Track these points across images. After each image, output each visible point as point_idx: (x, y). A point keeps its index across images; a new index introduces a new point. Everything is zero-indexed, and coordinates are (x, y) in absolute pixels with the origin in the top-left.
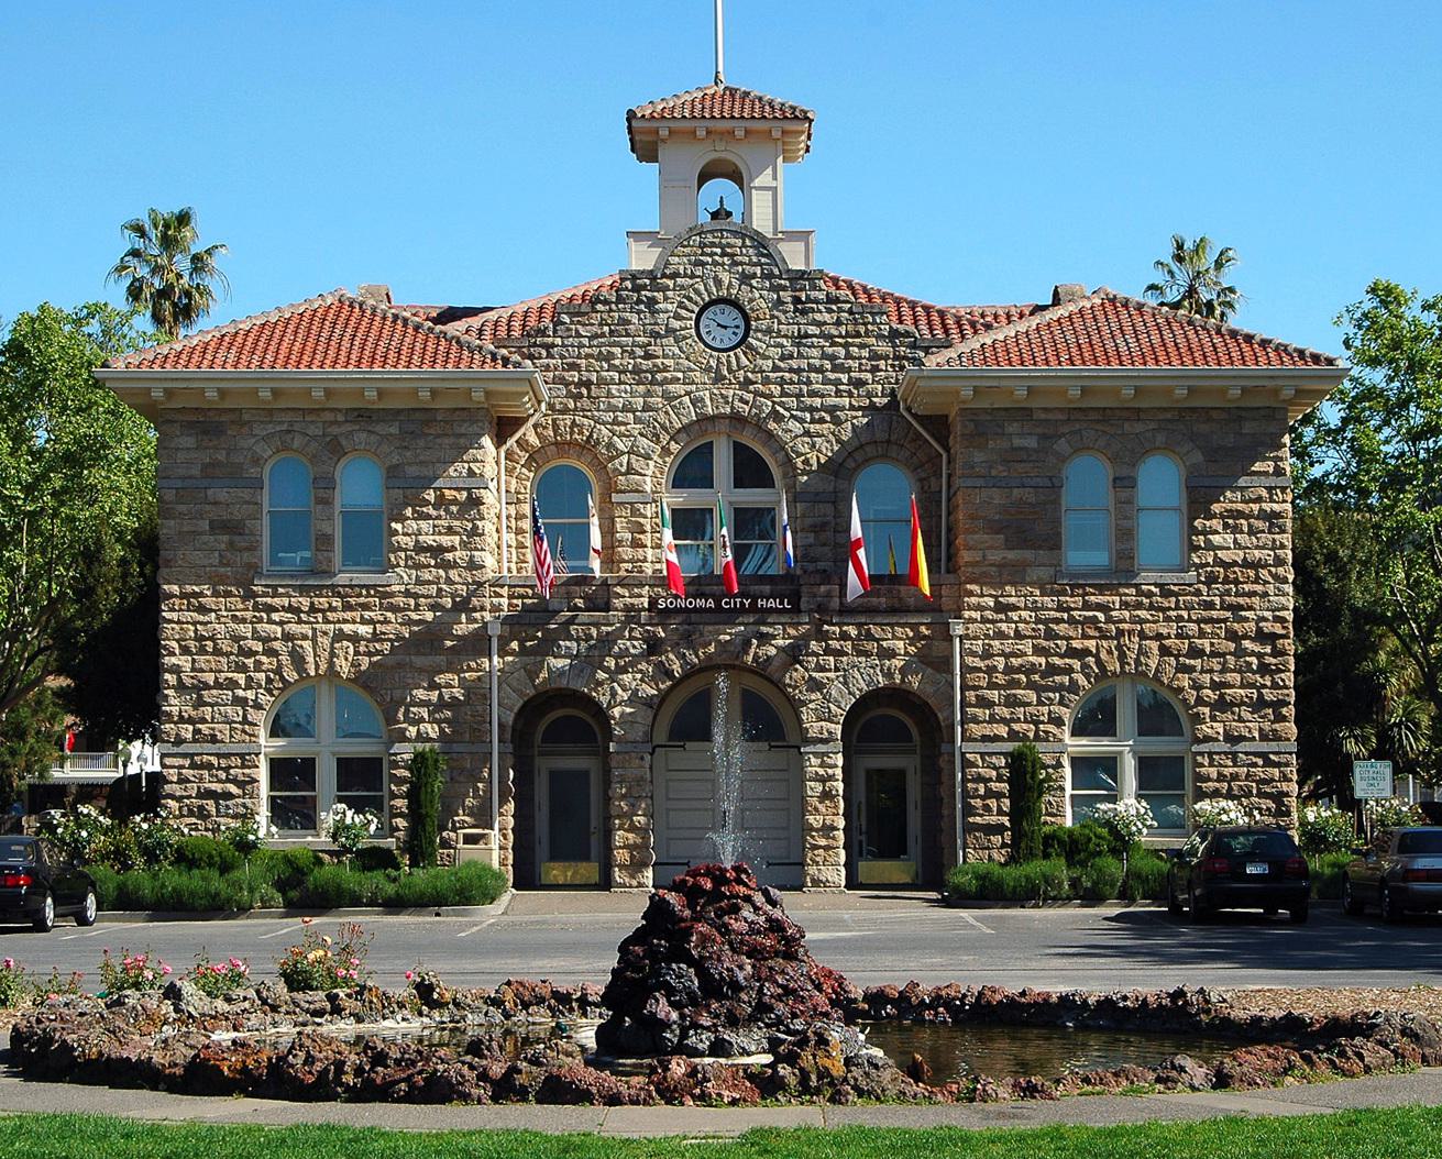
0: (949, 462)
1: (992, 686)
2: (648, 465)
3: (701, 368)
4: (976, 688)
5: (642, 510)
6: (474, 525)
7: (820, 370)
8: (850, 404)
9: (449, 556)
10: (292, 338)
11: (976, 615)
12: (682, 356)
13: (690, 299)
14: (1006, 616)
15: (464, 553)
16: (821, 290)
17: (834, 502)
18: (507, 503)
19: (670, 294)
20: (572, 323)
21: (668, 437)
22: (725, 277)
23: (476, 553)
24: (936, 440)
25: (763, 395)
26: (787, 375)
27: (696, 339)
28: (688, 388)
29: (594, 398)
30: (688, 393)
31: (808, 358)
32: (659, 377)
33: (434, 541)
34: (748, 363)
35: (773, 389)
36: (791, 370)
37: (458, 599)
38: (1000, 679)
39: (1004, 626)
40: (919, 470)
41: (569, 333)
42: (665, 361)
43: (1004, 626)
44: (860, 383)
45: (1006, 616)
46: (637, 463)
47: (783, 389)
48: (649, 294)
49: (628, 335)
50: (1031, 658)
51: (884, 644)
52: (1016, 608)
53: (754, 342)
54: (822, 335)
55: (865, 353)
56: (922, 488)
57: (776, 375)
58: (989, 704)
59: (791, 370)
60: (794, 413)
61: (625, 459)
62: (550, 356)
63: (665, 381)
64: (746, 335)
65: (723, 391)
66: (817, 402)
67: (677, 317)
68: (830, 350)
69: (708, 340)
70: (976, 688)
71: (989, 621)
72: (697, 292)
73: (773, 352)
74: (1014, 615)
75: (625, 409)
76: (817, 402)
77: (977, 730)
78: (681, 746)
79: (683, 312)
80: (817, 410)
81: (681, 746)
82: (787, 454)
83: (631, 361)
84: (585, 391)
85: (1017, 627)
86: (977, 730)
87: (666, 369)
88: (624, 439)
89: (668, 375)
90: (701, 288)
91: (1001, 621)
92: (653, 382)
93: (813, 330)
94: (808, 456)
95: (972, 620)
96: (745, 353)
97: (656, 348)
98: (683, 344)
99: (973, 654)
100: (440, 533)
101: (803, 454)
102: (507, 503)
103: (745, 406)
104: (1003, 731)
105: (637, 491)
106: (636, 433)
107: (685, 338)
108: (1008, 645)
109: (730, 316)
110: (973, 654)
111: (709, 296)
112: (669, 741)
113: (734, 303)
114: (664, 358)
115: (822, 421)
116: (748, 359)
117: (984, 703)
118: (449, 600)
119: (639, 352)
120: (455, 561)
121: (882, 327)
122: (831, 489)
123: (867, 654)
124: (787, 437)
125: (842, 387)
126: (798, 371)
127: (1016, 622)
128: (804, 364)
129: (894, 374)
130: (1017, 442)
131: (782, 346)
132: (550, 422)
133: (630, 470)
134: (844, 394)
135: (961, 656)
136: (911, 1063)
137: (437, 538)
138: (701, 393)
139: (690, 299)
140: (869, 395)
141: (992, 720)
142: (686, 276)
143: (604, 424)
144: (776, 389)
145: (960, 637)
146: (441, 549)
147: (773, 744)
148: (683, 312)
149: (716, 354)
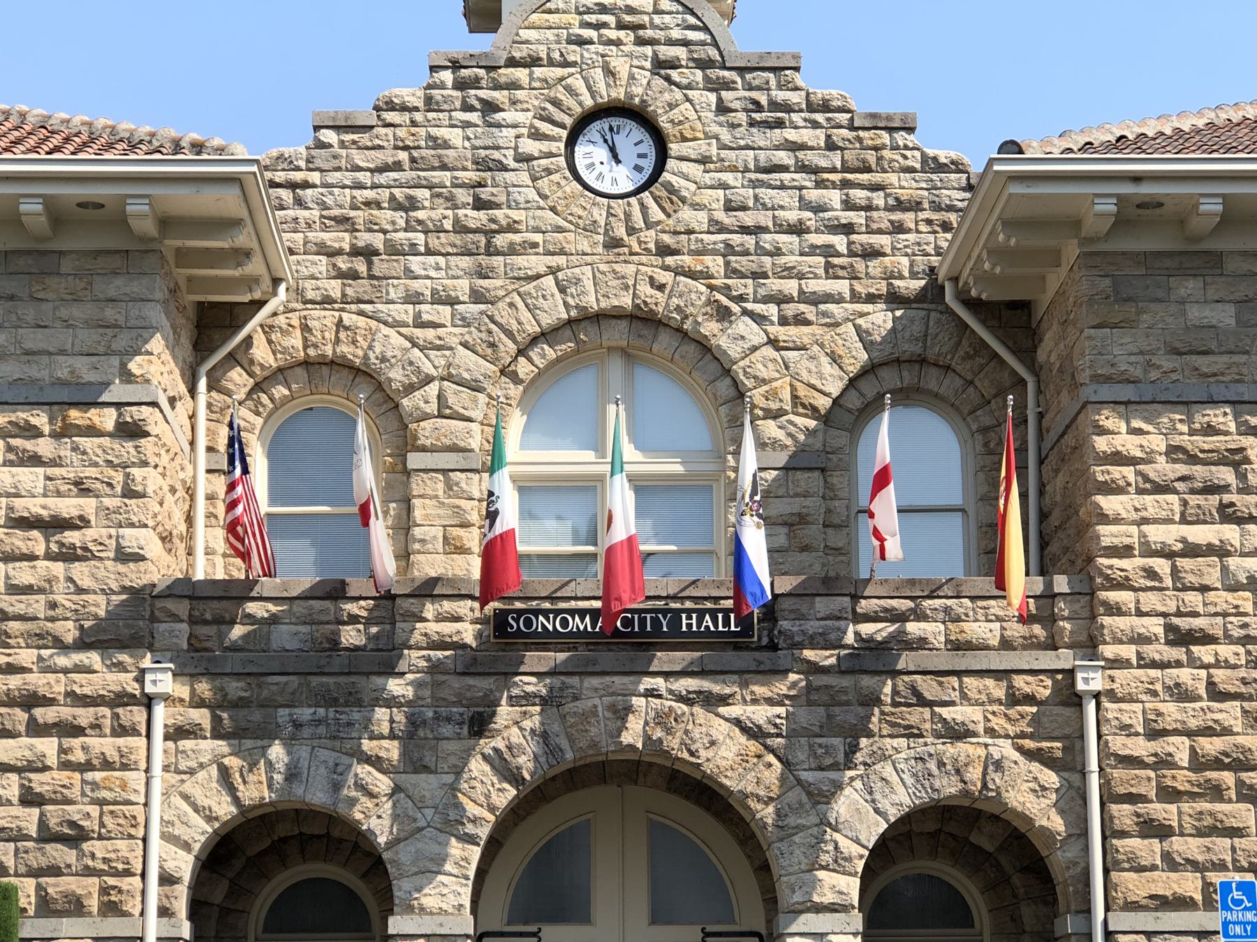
0: (1039, 391)
1: (1169, 794)
2: (475, 401)
3: (577, 226)
4: (1132, 798)
5: (463, 485)
6: (127, 475)
7: (798, 229)
8: (852, 290)
9: (72, 537)
10: (208, 616)
11: (1129, 652)
12: (542, 203)
13: (556, 103)
14: (1189, 652)
15: (104, 531)
16: (796, 89)
17: (823, 470)
18: (209, 471)
19: (520, 94)
20: (342, 144)
21: (512, 348)
22: (621, 65)
23: (126, 532)
24: (1015, 352)
25: (692, 275)
26: (736, 239)
27: (568, 174)
28: (554, 261)
29: (378, 278)
30: (553, 271)
31: (773, 209)
32: (500, 241)
33: (44, 507)
34: (662, 216)
35: (711, 264)
36: (745, 230)
37: (87, 624)
38: (1182, 779)
39: (1185, 675)
40: (979, 412)
41: (335, 163)
42: (509, 212)
43: (1185, 675)
44: (872, 253)
45: (1189, 652)
46: (458, 398)
47: (727, 264)
48: (483, 94)
49: (444, 167)
50: (1240, 740)
51: (945, 712)
52: (1207, 639)
53: (674, 180)
54: (803, 168)
55: (878, 199)
56: (986, 445)
57: (714, 237)
58: (1161, 831)
59: (745, 230)
60: (749, 306)
61: (433, 389)
62: (300, 203)
63: (512, 250)
64: (660, 167)
65: (617, 267)
66: (791, 287)
67: (536, 135)
68: (813, 195)
69: (589, 178)
70: (1132, 798)
71: (1154, 665)
72: (570, 90)
73: (707, 196)
74: (1204, 653)
75: (440, 299)
76: (791, 287)
77: (1133, 885)
78: (534, 935)
79: (545, 127)
80: (789, 300)
81: (534, 935)
82: (735, 383)
83: (449, 213)
84: (362, 268)
85: (1210, 676)
86: (1133, 885)
87: (511, 228)
88: (432, 353)
89: (517, 238)
90: (579, 84)
91: (1178, 664)
92: (491, 251)
93: (784, 157)
94: (774, 384)
95: (1118, 663)
96: (656, 199)
97: (495, 190)
98: (543, 184)
99: (1126, 729)
100: (59, 494)
101: (764, 382)
102: (209, 471)
103: (658, 294)
104: (1190, 885)
105: (454, 449)
106: (453, 342)
107: (549, 172)
108: (1193, 715)
109: (631, 138)
110: (1126, 729)
111: (593, 97)
112: (509, 923)
113: (639, 116)
114: (509, 207)
115: (801, 321)
116: (663, 209)
117: (1153, 829)
118: (70, 624)
119: (463, 196)
120: (86, 549)
121: (908, 153)
122: (819, 445)
123: (912, 733)
124: (734, 350)
125: (836, 261)
126: (758, 230)
127: (1207, 667)
128: (765, 219)
129: (931, 238)
130: (1196, 314)
131: (724, 186)
132: (295, 322)
133: (444, 411)
134: (841, 273)
135: (1099, 736)
136: (147, 428)
137: (52, 502)
138: (577, 270)
139: (556, 103)
140: (889, 276)
141: (1171, 863)
142: (551, 63)
143: (396, 324)
144: (715, 264)
145: (1097, 696)
146: (56, 525)
147: (710, 929)
148: (545, 127)
149: (605, 201)
